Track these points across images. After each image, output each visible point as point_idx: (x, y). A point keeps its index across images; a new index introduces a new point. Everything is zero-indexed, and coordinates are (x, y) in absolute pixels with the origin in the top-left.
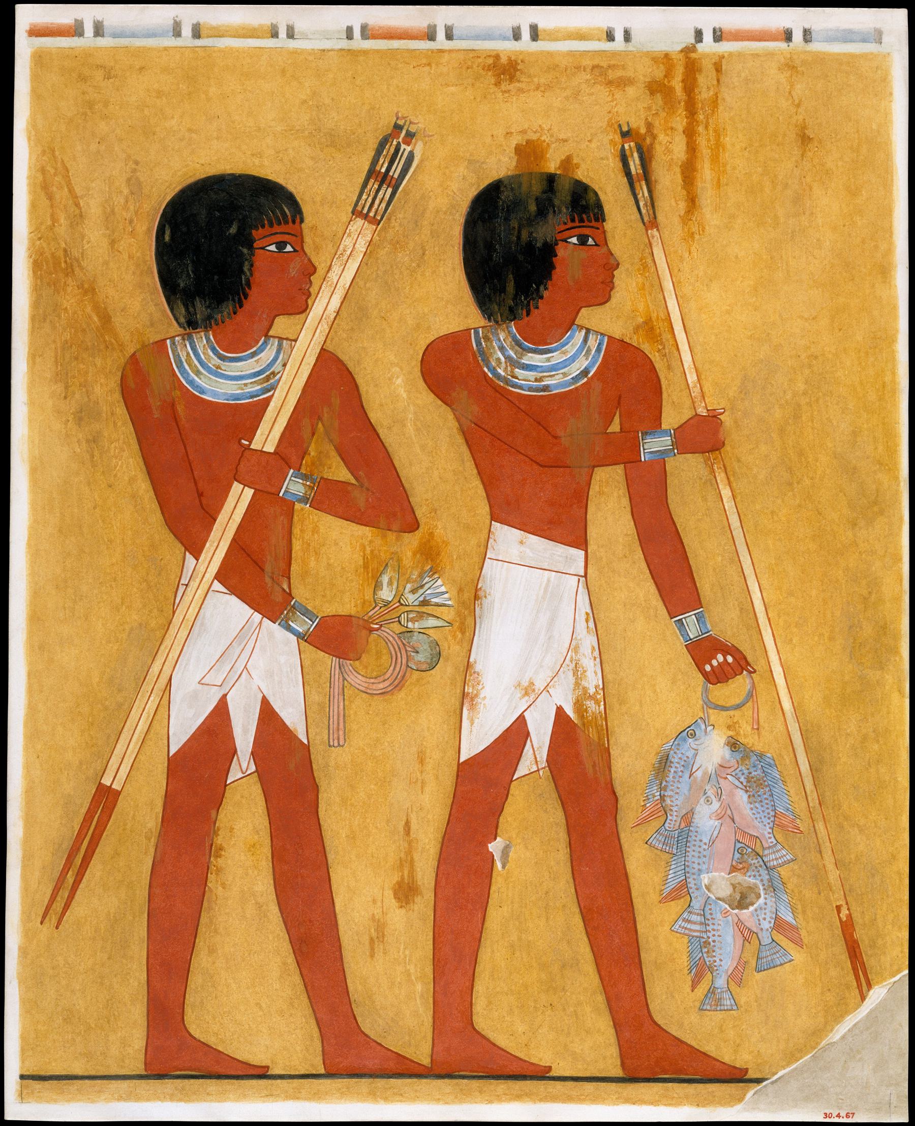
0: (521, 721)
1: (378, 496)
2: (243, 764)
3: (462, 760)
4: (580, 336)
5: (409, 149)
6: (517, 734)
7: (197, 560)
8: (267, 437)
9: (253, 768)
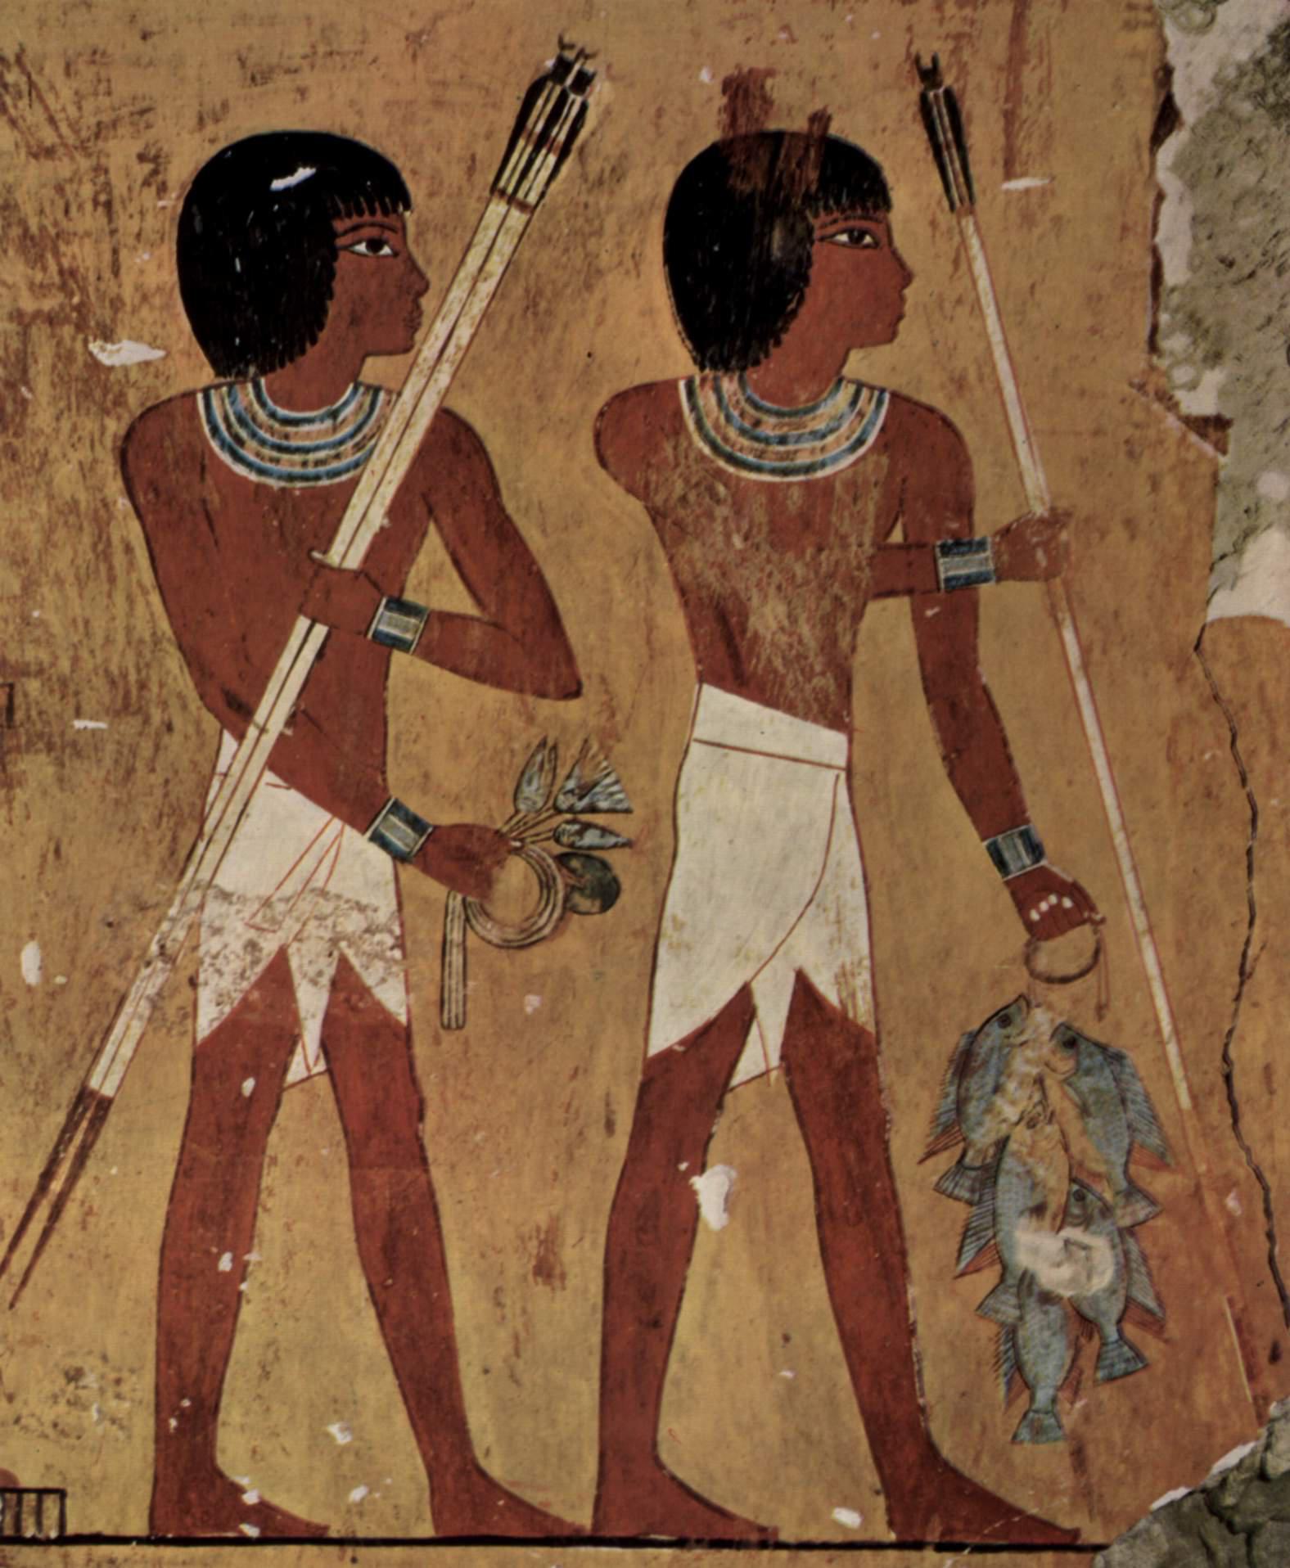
0: (745, 993)
1: (524, 640)
2: (306, 1060)
3: (657, 1045)
4: (845, 394)
5: (579, 100)
6: (739, 1013)
7: (240, 745)
8: (348, 549)
9: (321, 1066)
